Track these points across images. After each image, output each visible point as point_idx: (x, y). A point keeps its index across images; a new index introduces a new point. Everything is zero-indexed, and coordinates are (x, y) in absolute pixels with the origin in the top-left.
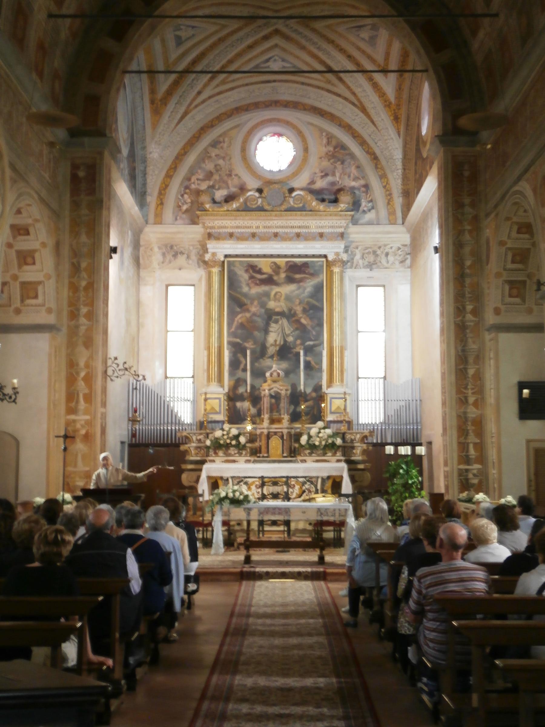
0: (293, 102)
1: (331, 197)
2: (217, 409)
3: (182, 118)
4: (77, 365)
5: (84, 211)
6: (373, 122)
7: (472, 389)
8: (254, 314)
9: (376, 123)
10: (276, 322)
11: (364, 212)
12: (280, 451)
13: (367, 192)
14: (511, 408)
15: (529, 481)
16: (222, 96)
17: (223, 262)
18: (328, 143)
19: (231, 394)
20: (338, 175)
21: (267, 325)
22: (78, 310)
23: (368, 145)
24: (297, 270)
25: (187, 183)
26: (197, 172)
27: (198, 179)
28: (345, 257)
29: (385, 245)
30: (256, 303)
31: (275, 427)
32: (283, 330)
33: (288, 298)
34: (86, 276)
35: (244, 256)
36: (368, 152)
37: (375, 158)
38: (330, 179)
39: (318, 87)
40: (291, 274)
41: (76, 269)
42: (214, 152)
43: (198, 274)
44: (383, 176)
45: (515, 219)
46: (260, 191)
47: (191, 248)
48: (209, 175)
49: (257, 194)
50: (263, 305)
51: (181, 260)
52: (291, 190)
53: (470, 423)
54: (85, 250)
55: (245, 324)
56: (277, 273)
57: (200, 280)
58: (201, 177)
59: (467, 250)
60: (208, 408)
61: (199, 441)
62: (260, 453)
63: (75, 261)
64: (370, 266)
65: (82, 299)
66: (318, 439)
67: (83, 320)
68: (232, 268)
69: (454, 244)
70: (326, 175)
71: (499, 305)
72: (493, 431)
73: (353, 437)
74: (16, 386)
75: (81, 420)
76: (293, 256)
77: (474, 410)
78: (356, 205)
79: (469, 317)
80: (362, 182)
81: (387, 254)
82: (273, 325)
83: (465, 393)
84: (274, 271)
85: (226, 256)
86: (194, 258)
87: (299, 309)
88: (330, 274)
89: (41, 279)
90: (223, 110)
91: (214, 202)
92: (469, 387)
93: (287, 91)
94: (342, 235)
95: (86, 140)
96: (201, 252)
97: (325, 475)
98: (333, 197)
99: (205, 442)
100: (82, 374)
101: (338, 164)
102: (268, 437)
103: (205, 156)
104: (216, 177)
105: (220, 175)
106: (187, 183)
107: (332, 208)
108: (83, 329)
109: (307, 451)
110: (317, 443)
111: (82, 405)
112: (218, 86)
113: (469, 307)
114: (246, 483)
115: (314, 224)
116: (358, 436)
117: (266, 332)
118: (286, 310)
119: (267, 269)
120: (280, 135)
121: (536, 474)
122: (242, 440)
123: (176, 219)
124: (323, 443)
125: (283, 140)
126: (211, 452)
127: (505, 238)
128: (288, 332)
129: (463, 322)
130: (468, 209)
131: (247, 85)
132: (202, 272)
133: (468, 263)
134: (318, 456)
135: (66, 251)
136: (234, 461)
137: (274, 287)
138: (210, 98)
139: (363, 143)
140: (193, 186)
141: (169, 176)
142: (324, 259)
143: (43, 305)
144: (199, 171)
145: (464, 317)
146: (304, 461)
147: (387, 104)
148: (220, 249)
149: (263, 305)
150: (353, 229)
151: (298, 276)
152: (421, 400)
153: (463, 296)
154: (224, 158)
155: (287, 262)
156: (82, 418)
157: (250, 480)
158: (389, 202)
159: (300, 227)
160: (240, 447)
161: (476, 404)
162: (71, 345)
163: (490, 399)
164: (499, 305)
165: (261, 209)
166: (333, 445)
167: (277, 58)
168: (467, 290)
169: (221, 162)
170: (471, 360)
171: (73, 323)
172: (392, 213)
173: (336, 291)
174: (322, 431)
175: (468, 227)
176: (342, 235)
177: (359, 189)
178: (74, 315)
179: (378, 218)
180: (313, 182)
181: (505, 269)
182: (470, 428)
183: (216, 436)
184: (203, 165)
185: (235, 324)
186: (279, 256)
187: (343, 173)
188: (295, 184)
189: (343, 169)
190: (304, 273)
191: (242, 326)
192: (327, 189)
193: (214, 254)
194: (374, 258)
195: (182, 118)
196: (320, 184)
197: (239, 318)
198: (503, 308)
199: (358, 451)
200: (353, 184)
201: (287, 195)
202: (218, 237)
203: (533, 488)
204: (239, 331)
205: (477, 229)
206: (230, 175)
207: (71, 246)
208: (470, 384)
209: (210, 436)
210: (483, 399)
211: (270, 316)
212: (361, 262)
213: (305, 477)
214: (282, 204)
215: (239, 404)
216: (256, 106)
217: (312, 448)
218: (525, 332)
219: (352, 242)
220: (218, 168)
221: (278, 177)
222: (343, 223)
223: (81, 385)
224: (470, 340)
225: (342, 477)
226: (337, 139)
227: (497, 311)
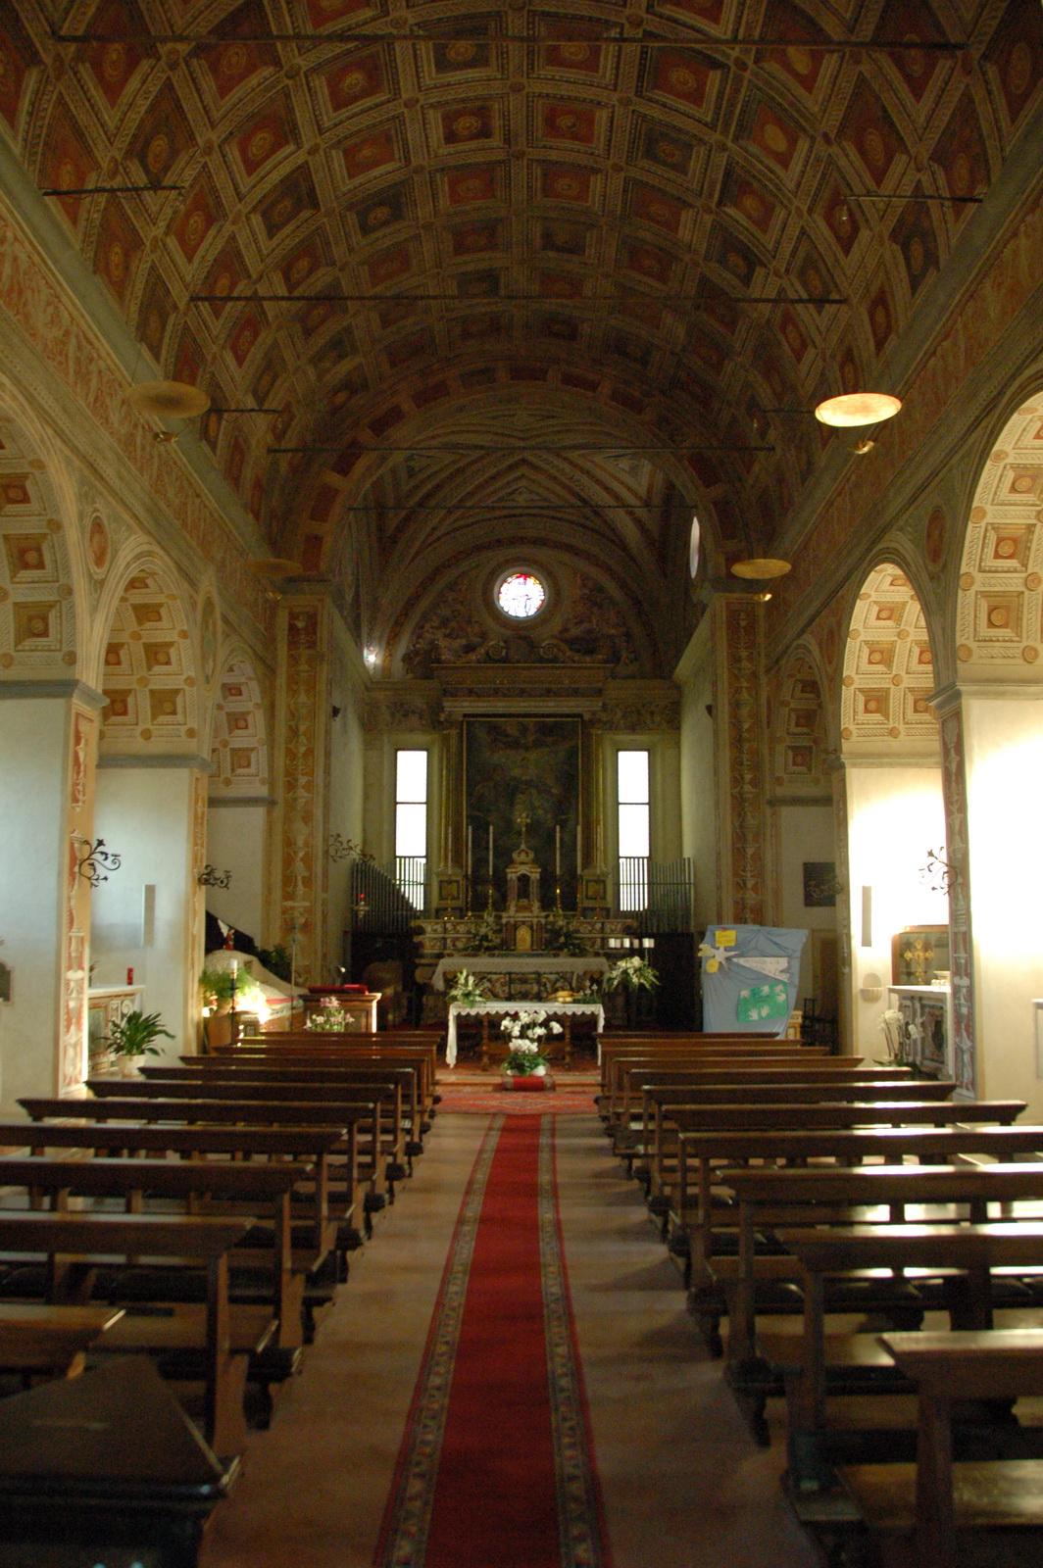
18: (584, 585)
38: (586, 626)
51: (414, 720)
59: (744, 711)
63: (292, 723)
67: (301, 792)
70: (581, 622)
76: (543, 716)
77: (754, 895)
79: (747, 788)
81: (652, 713)
85: (465, 716)
88: (587, 736)
94: (599, 692)
111: (301, 889)
113: (748, 777)
114: (489, 980)
119: (513, 731)
127: (788, 698)
129: (741, 794)
130: (745, 664)
133: (746, 726)
157: (494, 977)
161: (755, 889)
169: (459, 607)
170: (750, 837)
175: (745, 684)
193: (450, 714)
200: (613, 631)
207: (289, 706)
213: (557, 973)
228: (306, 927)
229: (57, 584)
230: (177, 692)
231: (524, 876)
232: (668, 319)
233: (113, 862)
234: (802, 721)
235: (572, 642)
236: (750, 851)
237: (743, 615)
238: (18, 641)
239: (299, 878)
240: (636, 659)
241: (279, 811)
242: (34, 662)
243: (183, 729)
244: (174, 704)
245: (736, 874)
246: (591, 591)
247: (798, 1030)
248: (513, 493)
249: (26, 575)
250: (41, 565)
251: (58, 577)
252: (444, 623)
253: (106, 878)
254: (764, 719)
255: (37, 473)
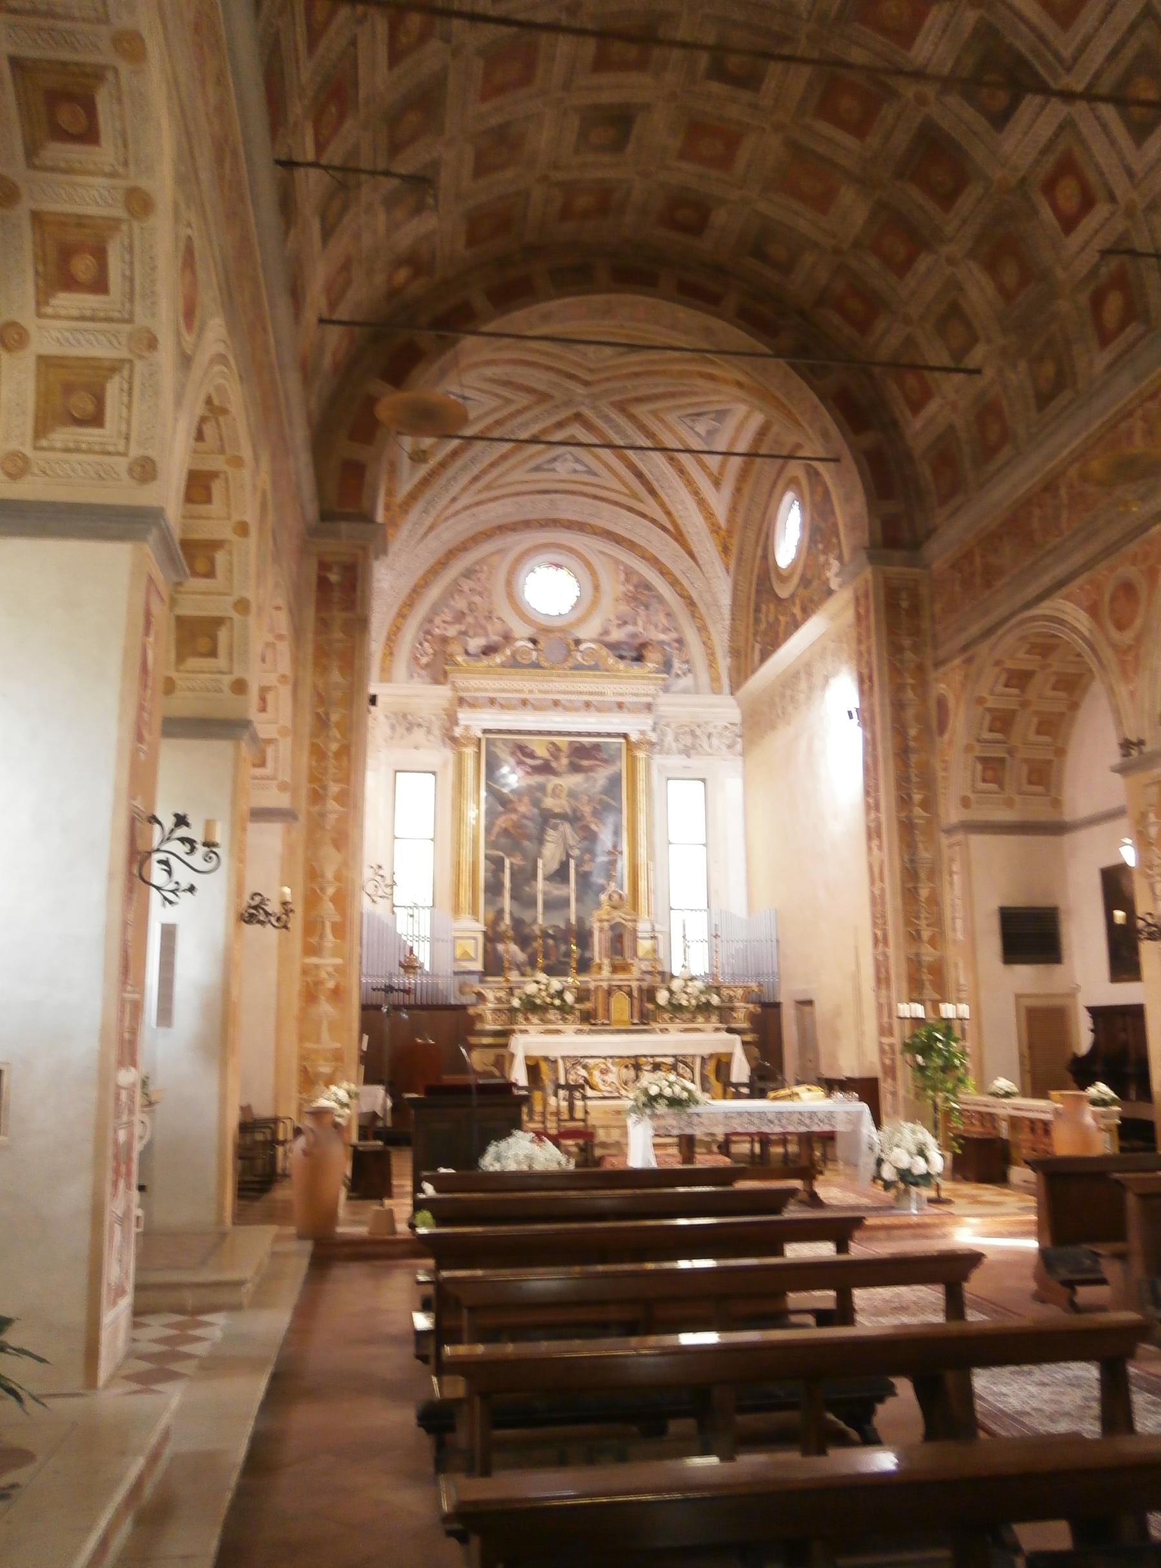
0: (578, 522)
1: (637, 653)
2: (473, 955)
3: (426, 534)
4: (323, 876)
5: (337, 635)
6: (692, 555)
7: (926, 918)
8: (525, 817)
9: (696, 555)
10: (555, 828)
11: (678, 676)
12: (626, 1016)
13: (680, 650)
14: (991, 943)
15: (1021, 1056)
16: (481, 508)
17: (480, 740)
18: (627, 580)
19: (490, 933)
20: (640, 623)
21: (542, 831)
22: (325, 788)
23: (681, 584)
24: (584, 754)
25: (428, 626)
26: (443, 612)
27: (444, 622)
28: (653, 737)
29: (706, 723)
30: (526, 799)
31: (620, 978)
32: (565, 838)
33: (572, 794)
34: (338, 736)
35: (510, 732)
36: (681, 596)
37: (690, 603)
38: (630, 628)
39: (616, 503)
40: (576, 760)
41: (322, 723)
42: (466, 585)
43: (440, 756)
44: (702, 629)
45: (1009, 664)
46: (534, 641)
47: (433, 718)
48: (460, 617)
49: (531, 645)
50: (536, 803)
51: (419, 735)
52: (578, 642)
53: (925, 970)
54: (337, 694)
55: (512, 830)
56: (556, 758)
57: (445, 765)
58: (448, 619)
59: (910, 713)
60: (459, 953)
61: (499, 1000)
62: (595, 1019)
63: (320, 710)
64: (687, 752)
65: (332, 770)
66: (685, 996)
67: (332, 805)
68: (492, 748)
69: (893, 704)
70: (625, 623)
71: (969, 794)
72: (962, 981)
73: (732, 993)
74: (289, 899)
75: (327, 965)
76: (579, 734)
77: (931, 950)
78: (667, 666)
79: (918, 811)
80: (674, 635)
81: (709, 736)
82: (551, 832)
83: (915, 924)
84: (552, 755)
85: (485, 731)
86: (437, 732)
87: (587, 810)
88: (633, 761)
89: (275, 735)
90: (480, 528)
91: (467, 653)
92: (922, 916)
93: (569, 508)
94: (649, 707)
95: (344, 526)
96: (448, 725)
97: (706, 1051)
98: (634, 654)
99: (509, 1002)
100: (330, 891)
101: (642, 611)
102: (609, 993)
103: (454, 589)
104: (470, 619)
105: (476, 618)
106: (428, 626)
107: (636, 669)
108: (332, 818)
109: (666, 1016)
110: (685, 1003)
111: (330, 939)
112: (480, 491)
113: (917, 797)
114: (585, 1067)
115: (610, 689)
116: (740, 992)
117: (541, 841)
118: (569, 811)
119: (542, 752)
120: (558, 566)
121: (1031, 1047)
122: (569, 998)
123: (412, 676)
124: (694, 1002)
125: (563, 573)
126: (520, 1017)
127: (985, 694)
128: (571, 842)
129: (909, 818)
130: (909, 655)
131: (518, 494)
132: (448, 754)
133: (913, 732)
134: (684, 1021)
135: (306, 695)
136: (558, 1032)
137: (552, 777)
138: (466, 508)
139: (674, 583)
140: (437, 631)
141: (402, 615)
142: (622, 740)
143: (274, 778)
144: (446, 610)
145: (911, 811)
146: (664, 1031)
147: (715, 529)
148: (476, 721)
149: (536, 803)
150: (663, 698)
151: (585, 763)
152: (778, 941)
153: (907, 779)
154: (480, 594)
155: (571, 743)
156: (328, 961)
157: (591, 1062)
158: (712, 664)
159: (591, 693)
160: (564, 1009)
161: (933, 942)
162: (312, 843)
163: (957, 931)
164: (969, 794)
165: (536, 665)
166: (708, 1004)
167: (569, 457)
168: (913, 772)
169: (477, 599)
170: (923, 875)
171: (316, 808)
172: (715, 679)
173: (641, 785)
174: (690, 983)
175: (910, 681)
176: (649, 707)
177: (669, 644)
178: (317, 796)
179: (696, 685)
180: (606, 632)
181: (979, 741)
182: (926, 977)
183: (528, 992)
184: (452, 603)
185: (496, 830)
186: (560, 733)
187: (648, 621)
188: (581, 635)
189: (648, 616)
190: (596, 759)
191: (505, 832)
192: (626, 643)
193: (467, 728)
194: (692, 741)
195: (426, 534)
196: (617, 635)
197: (502, 822)
198: (972, 796)
199: (740, 1014)
200: (662, 637)
201: (573, 647)
202: (473, 705)
203: (1028, 1068)
204: (503, 840)
205: (922, 686)
206: (489, 618)
207: (315, 687)
208: (923, 911)
209: (517, 992)
210: (942, 933)
211: (547, 818)
212: (674, 745)
213: (674, 1056)
214: (565, 660)
215: (500, 947)
216: (527, 525)
217: (676, 1009)
218: (995, 833)
219: (662, 717)
220: (472, 607)
221: (558, 623)
222: (651, 689)
223: (328, 909)
224: (920, 846)
225: (730, 1055)
226: (638, 573)
227: (965, 803)
228: (337, 994)
229: (127, 328)
230: (218, 622)
231: (619, 924)
232: (847, 195)
233: (207, 859)
234: (998, 724)
235: (613, 647)
236: (924, 893)
237: (904, 595)
238: (42, 428)
239: (328, 926)
240: (689, 671)
241: (300, 827)
242: (70, 470)
243: (227, 680)
244: (214, 639)
245: (908, 922)
246: (636, 587)
247: (1116, 1134)
248: (555, 459)
249: (67, 301)
250: (100, 286)
251: (131, 313)
252: (460, 617)
253: (192, 889)
254: (934, 723)
255: (124, 68)
